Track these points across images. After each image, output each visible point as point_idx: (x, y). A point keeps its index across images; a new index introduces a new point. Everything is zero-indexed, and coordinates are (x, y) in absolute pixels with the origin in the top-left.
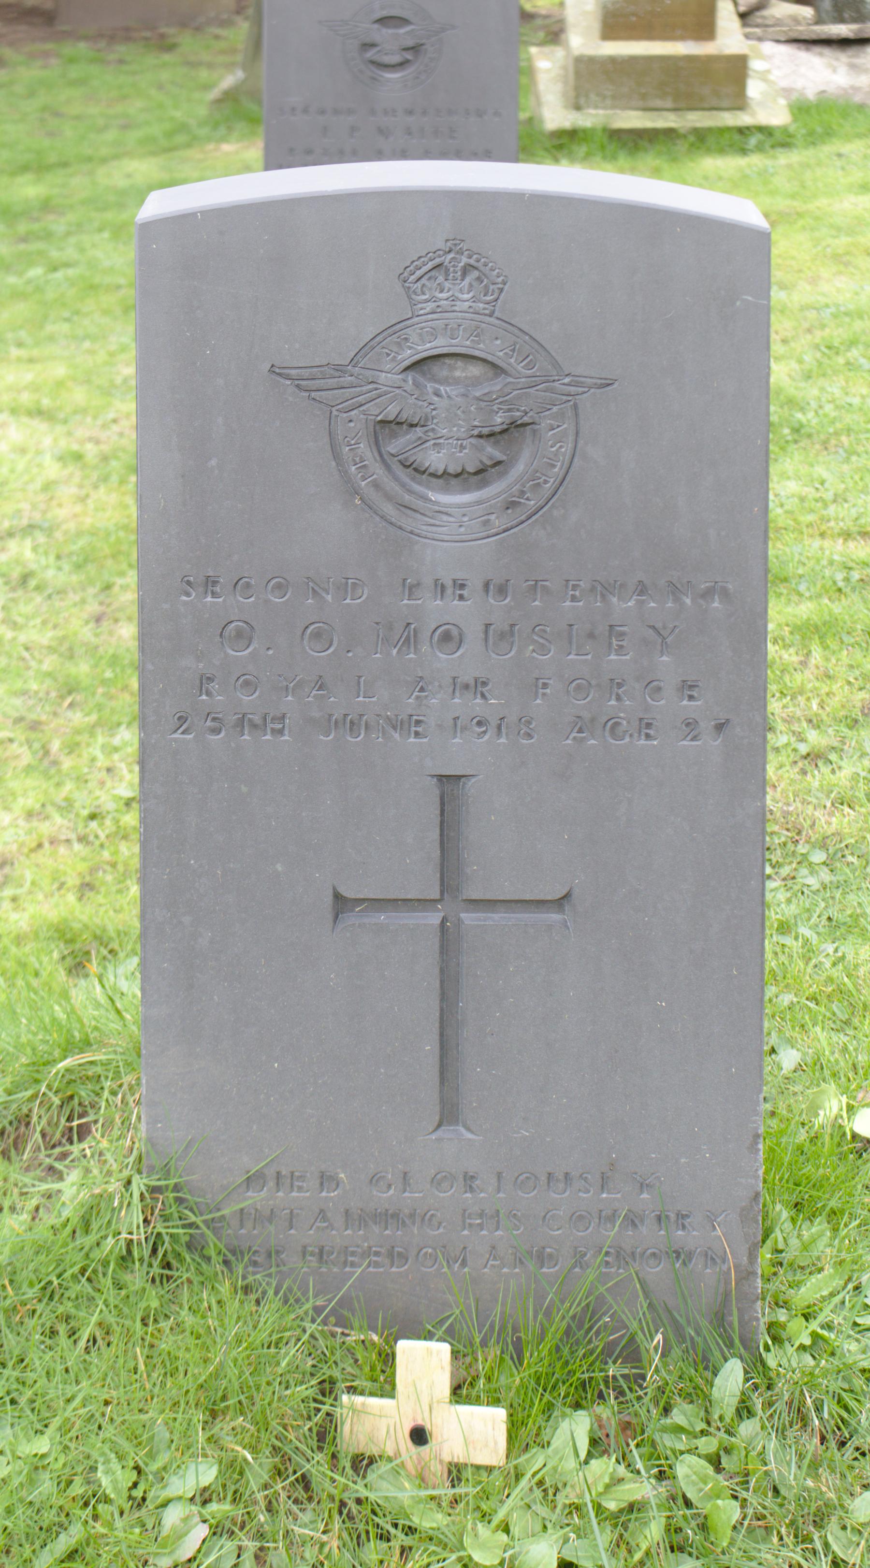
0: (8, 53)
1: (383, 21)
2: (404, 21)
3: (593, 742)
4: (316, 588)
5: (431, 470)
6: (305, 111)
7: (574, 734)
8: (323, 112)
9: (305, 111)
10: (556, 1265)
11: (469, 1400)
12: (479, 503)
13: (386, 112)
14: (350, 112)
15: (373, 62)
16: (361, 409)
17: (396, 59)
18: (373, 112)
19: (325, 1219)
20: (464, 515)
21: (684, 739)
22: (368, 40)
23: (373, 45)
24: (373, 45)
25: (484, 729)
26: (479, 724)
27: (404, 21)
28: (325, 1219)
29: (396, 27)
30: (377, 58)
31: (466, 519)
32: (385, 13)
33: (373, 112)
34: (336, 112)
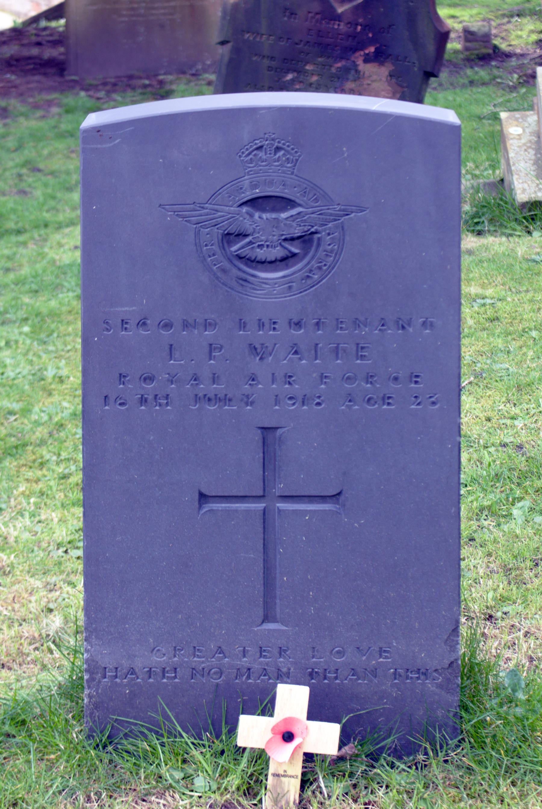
0: (13, 103)
1: (253, 202)
2: (289, 203)
3: (356, 407)
4: (202, 205)
5: (257, 259)
6: (142, 324)
7: (347, 403)
8: (168, 326)
9: (142, 324)
10: (343, 656)
11: (304, 761)
12: (284, 277)
13: (261, 325)
14: (207, 325)
15: (240, 258)
16: (217, 227)
17: (277, 253)
18: (242, 325)
19: (222, 652)
20: (276, 284)
21: (413, 404)
22: (232, 229)
23: (242, 235)
24: (242, 235)
25: (294, 401)
26: (290, 398)
27: (289, 203)
28: (222, 652)
29: (274, 210)
30: (243, 252)
31: (277, 286)
32: (257, 192)
33: (242, 325)
34: (186, 325)
